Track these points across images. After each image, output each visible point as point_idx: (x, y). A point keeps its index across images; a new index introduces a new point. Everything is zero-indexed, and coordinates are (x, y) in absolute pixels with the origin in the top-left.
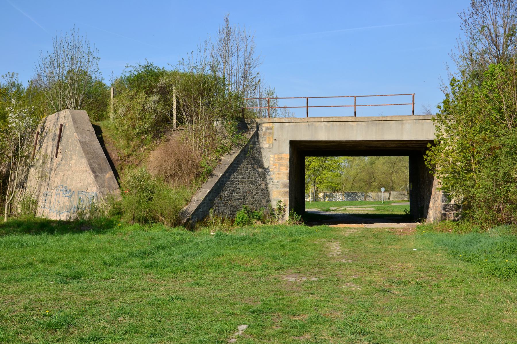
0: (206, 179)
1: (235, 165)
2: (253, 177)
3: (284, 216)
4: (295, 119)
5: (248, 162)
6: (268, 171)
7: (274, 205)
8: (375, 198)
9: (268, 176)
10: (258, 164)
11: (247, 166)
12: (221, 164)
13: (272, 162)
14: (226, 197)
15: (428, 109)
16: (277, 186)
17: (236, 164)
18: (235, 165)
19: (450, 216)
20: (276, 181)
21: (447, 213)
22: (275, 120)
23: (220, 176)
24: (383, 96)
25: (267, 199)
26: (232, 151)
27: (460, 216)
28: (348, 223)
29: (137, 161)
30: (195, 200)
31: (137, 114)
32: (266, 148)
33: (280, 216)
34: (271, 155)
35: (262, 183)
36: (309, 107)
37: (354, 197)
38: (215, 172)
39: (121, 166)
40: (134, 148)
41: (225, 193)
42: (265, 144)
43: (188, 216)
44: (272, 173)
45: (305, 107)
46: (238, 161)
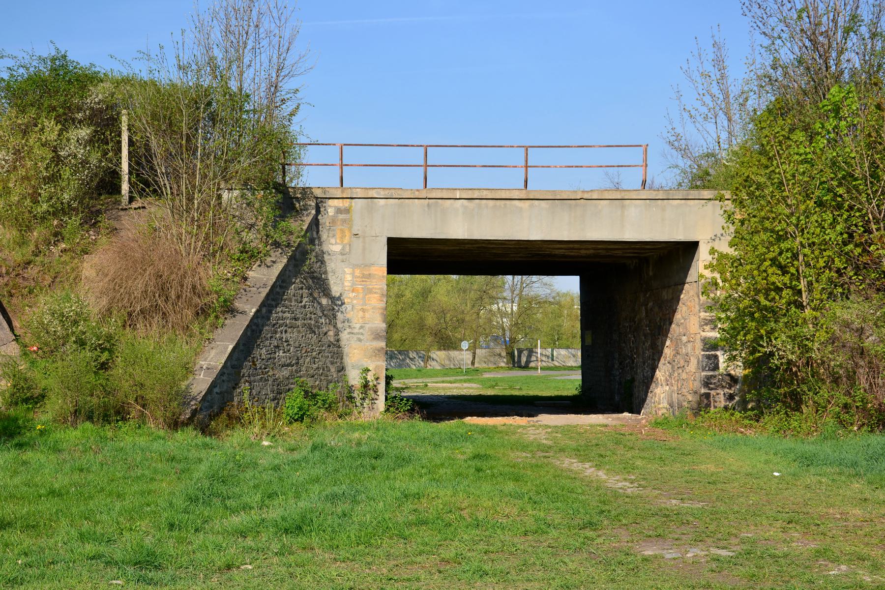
0: (222, 321)
1: (278, 289)
2: (313, 316)
3: (376, 401)
4: (399, 192)
5: (302, 283)
6: (340, 303)
7: (354, 378)
8: (443, 363)
9: (339, 314)
10: (320, 288)
11: (301, 292)
12: (250, 287)
13: (350, 284)
14: (263, 359)
15: (616, 180)
16: (359, 336)
17: (281, 287)
18: (278, 289)
19: (717, 399)
20: (358, 326)
21: (713, 392)
22: (357, 193)
23: (252, 314)
24: (585, 148)
25: (339, 364)
26: (269, 259)
27: (737, 398)
28: (483, 416)
29: (47, 277)
30: (202, 368)
31: (42, 169)
32: (335, 253)
33: (367, 401)
34: (346, 270)
35: (329, 330)
36: (429, 166)
37: (404, 360)
38: (237, 304)
39: (9, 288)
40: (37, 246)
41: (261, 352)
42: (332, 244)
43: (192, 403)
44: (349, 307)
45: (421, 166)
46: (283, 281)
